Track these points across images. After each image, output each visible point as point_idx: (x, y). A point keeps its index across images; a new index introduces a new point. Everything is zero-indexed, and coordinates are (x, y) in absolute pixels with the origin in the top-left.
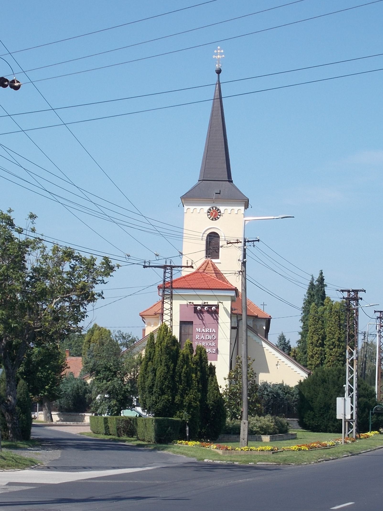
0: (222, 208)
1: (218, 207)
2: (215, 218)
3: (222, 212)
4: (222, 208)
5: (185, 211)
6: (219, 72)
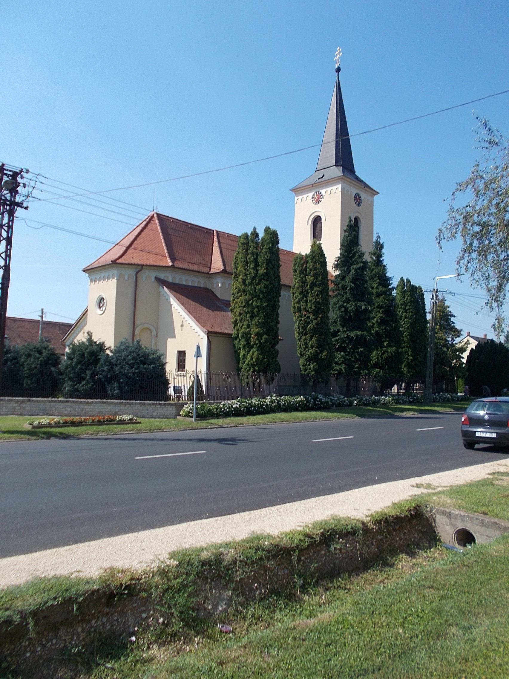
0: (323, 191)
1: (320, 191)
2: (318, 202)
3: (323, 195)
4: (323, 191)
5: (296, 202)
6: (338, 70)
